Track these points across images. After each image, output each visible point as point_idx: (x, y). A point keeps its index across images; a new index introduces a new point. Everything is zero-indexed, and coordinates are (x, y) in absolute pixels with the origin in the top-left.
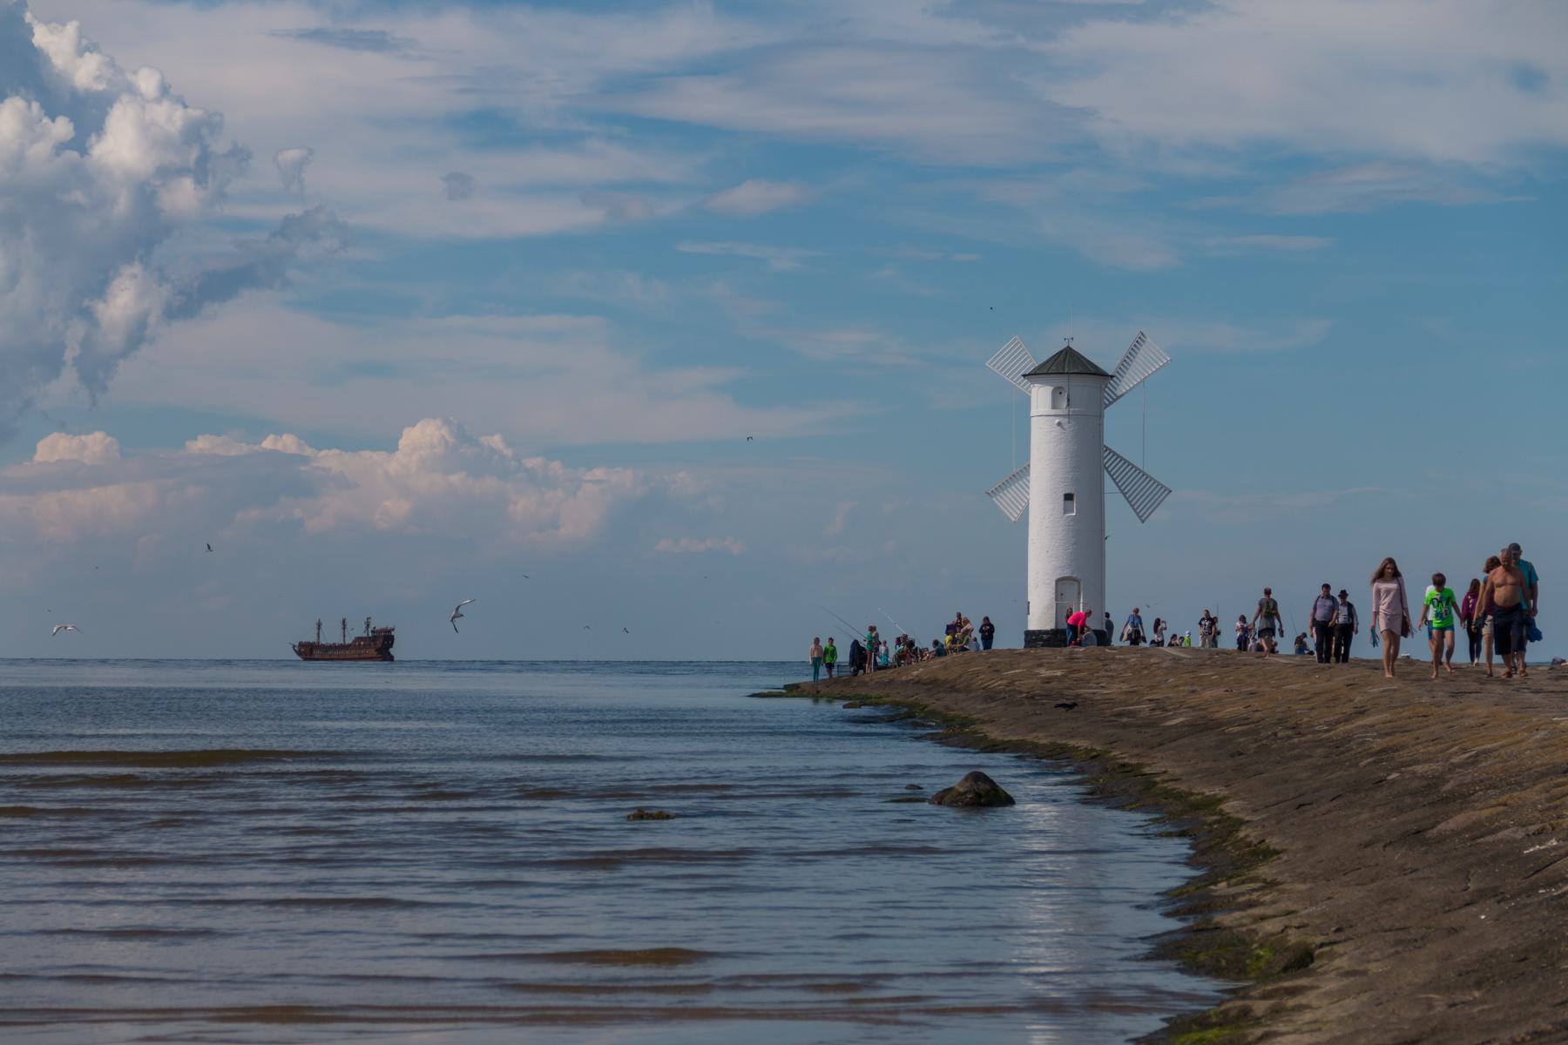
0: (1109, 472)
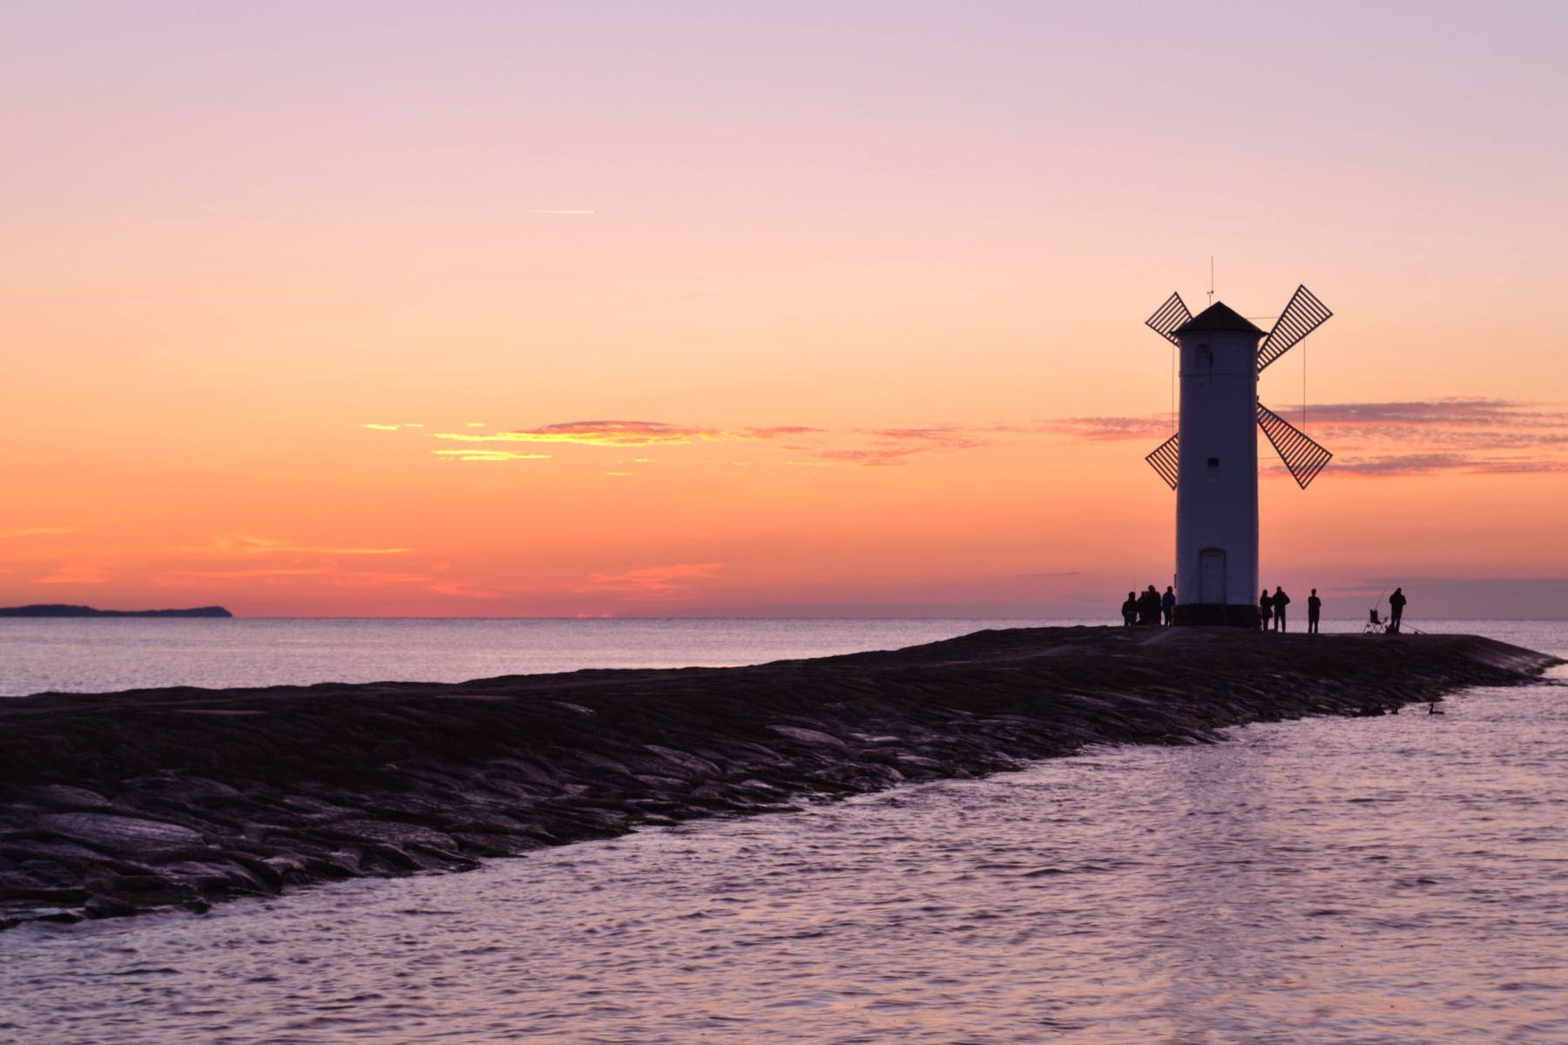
0: (1261, 424)
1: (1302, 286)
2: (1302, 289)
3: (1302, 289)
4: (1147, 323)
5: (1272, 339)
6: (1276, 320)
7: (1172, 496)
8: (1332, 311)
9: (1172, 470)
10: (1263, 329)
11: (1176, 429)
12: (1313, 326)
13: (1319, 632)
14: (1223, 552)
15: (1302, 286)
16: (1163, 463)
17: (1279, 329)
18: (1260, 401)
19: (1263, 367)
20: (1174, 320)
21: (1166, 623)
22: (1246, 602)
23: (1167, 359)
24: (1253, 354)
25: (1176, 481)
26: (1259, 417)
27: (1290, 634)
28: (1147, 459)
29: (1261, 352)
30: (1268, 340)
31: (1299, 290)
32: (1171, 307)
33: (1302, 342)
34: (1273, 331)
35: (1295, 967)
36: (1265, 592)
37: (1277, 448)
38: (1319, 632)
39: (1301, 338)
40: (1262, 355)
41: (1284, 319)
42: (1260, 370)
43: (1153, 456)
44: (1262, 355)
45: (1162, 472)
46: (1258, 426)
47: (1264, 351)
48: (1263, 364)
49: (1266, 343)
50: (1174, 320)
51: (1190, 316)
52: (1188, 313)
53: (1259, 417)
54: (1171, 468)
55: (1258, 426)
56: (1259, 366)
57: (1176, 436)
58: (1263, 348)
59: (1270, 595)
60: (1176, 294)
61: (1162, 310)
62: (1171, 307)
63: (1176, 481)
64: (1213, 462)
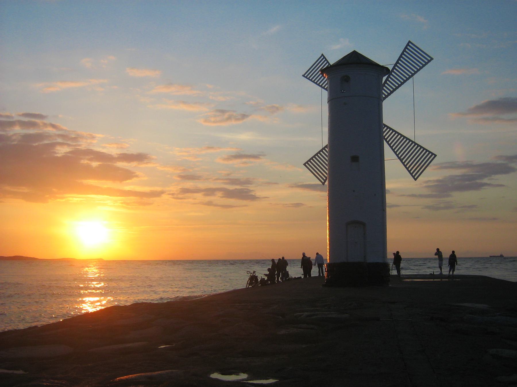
4: (303, 76)
5: (391, 76)
8: (432, 57)
14: (363, 224)
19: (386, 97)
22: (380, 261)
24: (380, 86)
27: (454, 275)
28: (305, 164)
30: (389, 77)
33: (411, 79)
35: (190, 290)
37: (395, 153)
39: (410, 77)
40: (393, 73)
42: (384, 99)
43: (311, 161)
44: (393, 73)
48: (387, 94)
49: (387, 80)
51: (329, 64)
52: (328, 62)
56: (384, 96)
57: (326, 146)
58: (385, 82)
60: (322, 55)
61: (312, 69)
64: (355, 159)
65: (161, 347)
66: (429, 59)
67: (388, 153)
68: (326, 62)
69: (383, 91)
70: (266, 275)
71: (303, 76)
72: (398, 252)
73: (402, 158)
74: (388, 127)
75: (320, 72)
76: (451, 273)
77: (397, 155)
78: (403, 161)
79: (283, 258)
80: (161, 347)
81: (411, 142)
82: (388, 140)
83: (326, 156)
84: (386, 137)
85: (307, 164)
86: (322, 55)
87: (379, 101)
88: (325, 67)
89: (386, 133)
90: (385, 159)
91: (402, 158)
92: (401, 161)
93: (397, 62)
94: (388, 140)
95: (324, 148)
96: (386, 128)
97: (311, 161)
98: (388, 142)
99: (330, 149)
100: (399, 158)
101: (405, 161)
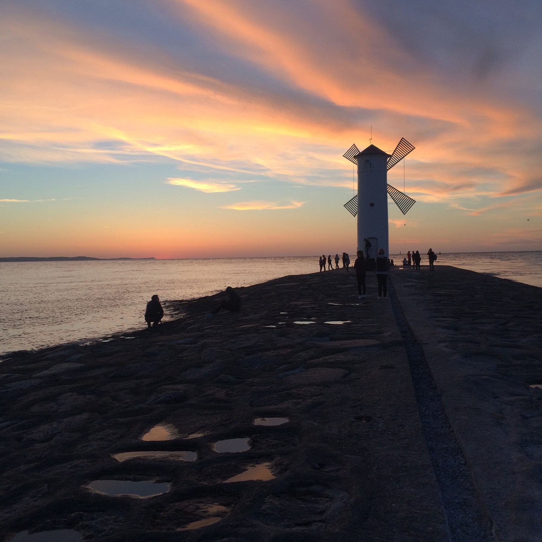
1: (403, 138)
2: (403, 139)
3: (403, 139)
4: (343, 156)
6: (393, 151)
7: (355, 220)
9: (355, 209)
10: (388, 153)
11: (356, 193)
12: (407, 153)
13: (326, 270)
14: (376, 239)
15: (403, 138)
16: (352, 211)
17: (391, 160)
18: (388, 183)
19: (389, 169)
20: (352, 204)
21: (414, 264)
23: (352, 167)
25: (357, 210)
26: (388, 190)
29: (388, 162)
31: (402, 140)
32: (350, 155)
34: (393, 154)
36: (413, 252)
38: (326, 270)
41: (396, 151)
42: (388, 170)
44: (388, 164)
45: (352, 213)
46: (388, 193)
47: (389, 162)
49: (390, 159)
50: (352, 204)
51: (360, 152)
52: (359, 151)
53: (388, 190)
54: (355, 208)
55: (388, 193)
58: (389, 161)
59: (415, 253)
60: (354, 144)
62: (350, 155)
63: (357, 210)
65: (133, 338)
66: (413, 148)
67: (390, 200)
68: (401, 209)
69: (388, 166)
70: (413, 252)
71: (343, 156)
72: (431, 249)
73: (397, 202)
74: (390, 186)
75: (353, 158)
76: (323, 270)
77: (395, 201)
78: (398, 204)
79: (417, 252)
80: (133, 338)
81: (402, 194)
82: (390, 193)
83: (356, 201)
84: (389, 191)
85: (345, 206)
86: (354, 144)
87: (385, 171)
88: (356, 155)
89: (389, 189)
90: (388, 203)
91: (397, 202)
92: (397, 204)
93: (396, 150)
94: (390, 193)
95: (355, 197)
96: (389, 186)
97: (348, 204)
98: (390, 194)
99: (358, 198)
100: (396, 203)
101: (396, 200)
